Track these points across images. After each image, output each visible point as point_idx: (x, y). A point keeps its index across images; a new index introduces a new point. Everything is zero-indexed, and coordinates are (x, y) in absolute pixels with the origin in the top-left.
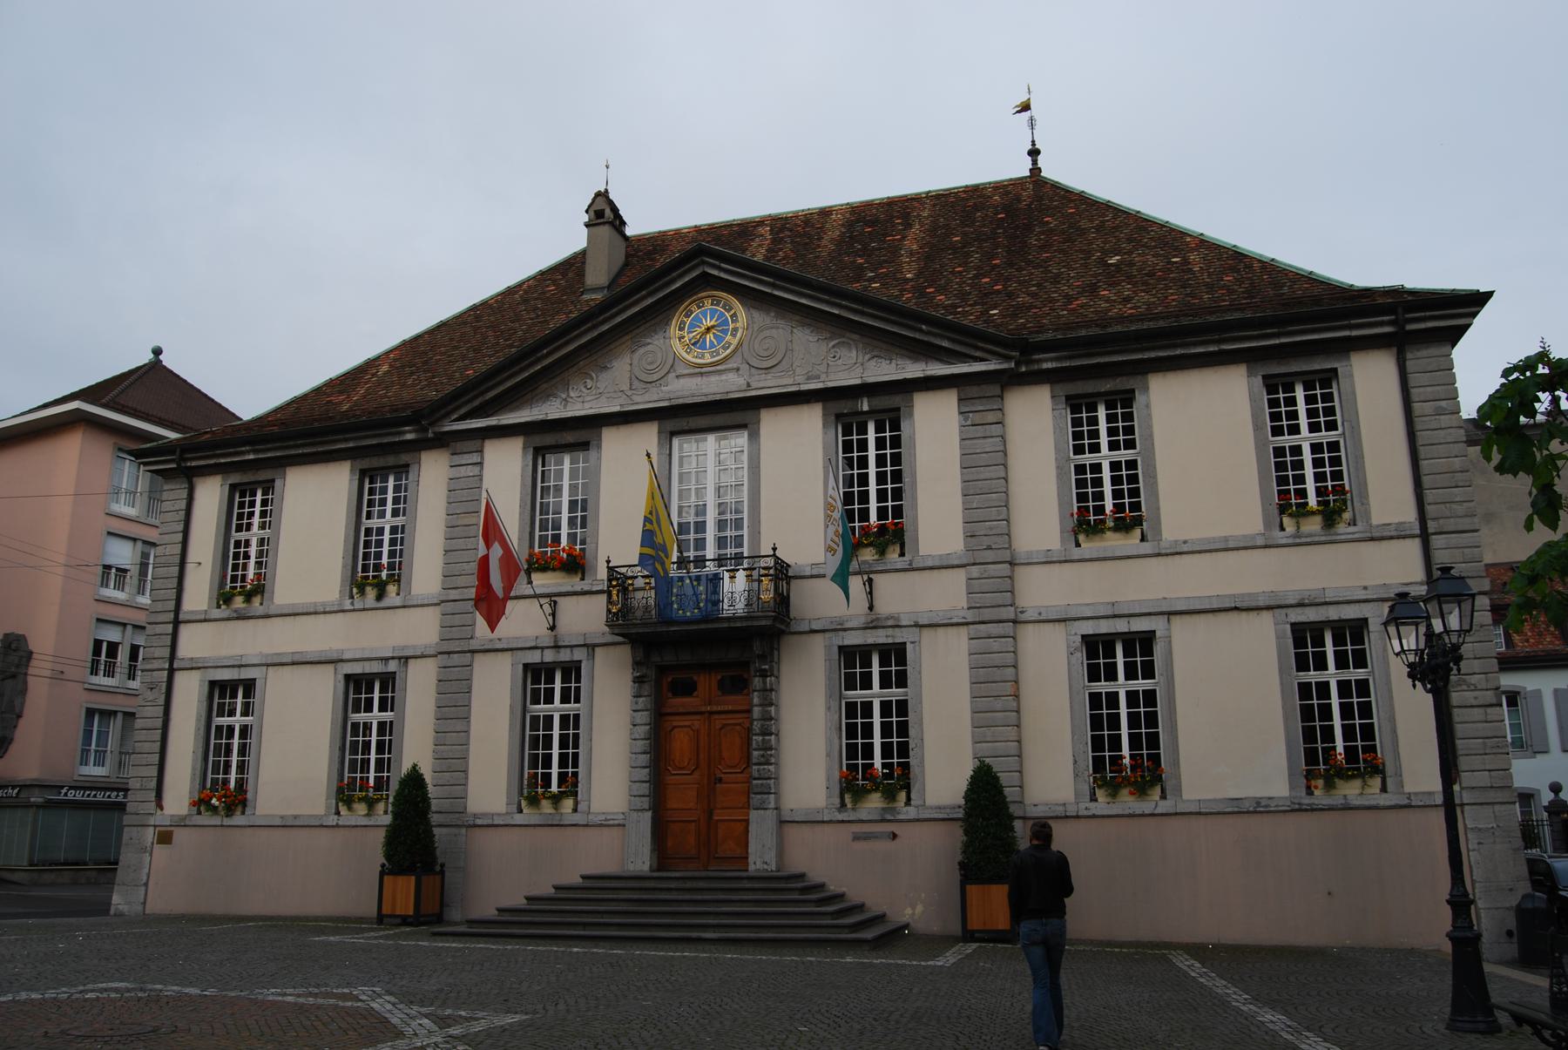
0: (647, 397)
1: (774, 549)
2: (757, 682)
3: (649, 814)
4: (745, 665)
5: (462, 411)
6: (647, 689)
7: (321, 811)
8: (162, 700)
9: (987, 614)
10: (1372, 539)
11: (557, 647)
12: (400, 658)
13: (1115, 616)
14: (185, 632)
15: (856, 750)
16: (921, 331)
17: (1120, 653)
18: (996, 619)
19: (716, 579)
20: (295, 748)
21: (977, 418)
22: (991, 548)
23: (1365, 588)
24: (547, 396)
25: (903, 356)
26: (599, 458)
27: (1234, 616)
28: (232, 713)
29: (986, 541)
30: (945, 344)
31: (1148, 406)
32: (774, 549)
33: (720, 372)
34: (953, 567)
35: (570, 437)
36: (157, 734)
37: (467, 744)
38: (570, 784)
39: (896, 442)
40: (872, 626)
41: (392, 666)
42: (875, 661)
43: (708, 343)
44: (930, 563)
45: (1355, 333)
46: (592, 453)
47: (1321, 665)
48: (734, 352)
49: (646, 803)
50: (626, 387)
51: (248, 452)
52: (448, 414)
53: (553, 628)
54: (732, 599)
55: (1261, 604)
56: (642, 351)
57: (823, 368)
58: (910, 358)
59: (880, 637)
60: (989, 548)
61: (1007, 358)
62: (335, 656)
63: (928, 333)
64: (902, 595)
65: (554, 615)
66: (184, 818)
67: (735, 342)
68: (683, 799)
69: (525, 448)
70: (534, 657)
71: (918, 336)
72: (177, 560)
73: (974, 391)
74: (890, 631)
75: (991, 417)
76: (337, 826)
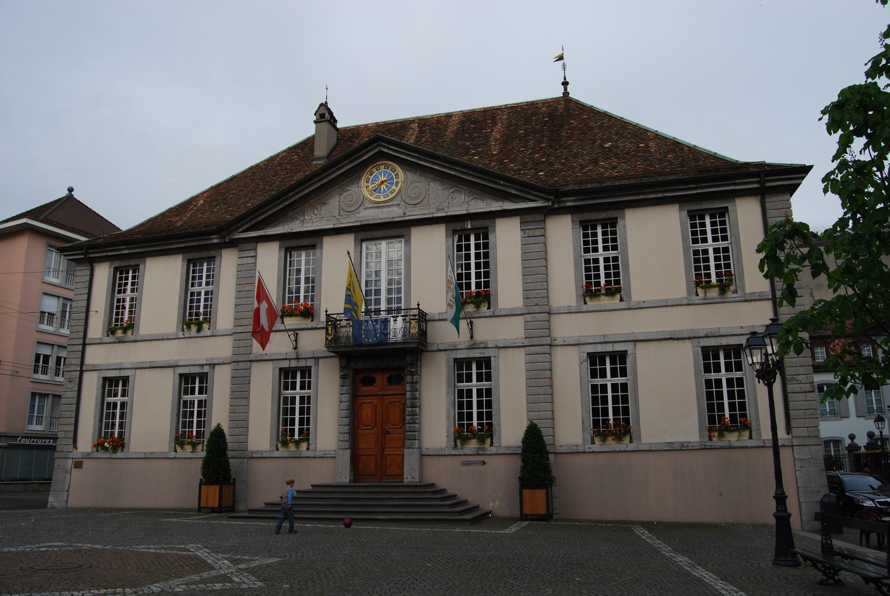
0: (348, 220)
1: (418, 305)
2: (409, 378)
3: (349, 451)
4: (402, 369)
5: (245, 227)
6: (348, 381)
7: (89, 450)
8: (76, 388)
9: (536, 341)
10: (746, 301)
11: (298, 359)
12: (210, 365)
13: (605, 342)
14: (89, 350)
15: (463, 415)
16: (500, 184)
17: (608, 363)
18: (540, 344)
19: (386, 322)
20: (151, 415)
21: (531, 233)
22: (538, 305)
23: (742, 328)
24: (293, 219)
25: (490, 198)
26: (322, 254)
27: (670, 342)
28: (116, 395)
29: (535, 301)
30: (513, 192)
31: (624, 227)
32: (418, 305)
33: (389, 206)
34: (517, 315)
35: (305, 242)
36: (74, 407)
37: (248, 412)
38: (305, 434)
39: (486, 246)
40: (473, 347)
41: (206, 369)
42: (475, 367)
43: (382, 190)
44: (504, 313)
45: (738, 188)
46: (318, 251)
47: (717, 369)
48: (397, 195)
49: (347, 445)
50: (336, 214)
51: (124, 249)
52: (237, 229)
53: (295, 348)
54: (395, 333)
55: (685, 336)
56: (345, 194)
57: (446, 204)
58: (494, 199)
59: (476, 354)
60: (537, 305)
61: (547, 200)
62: (173, 364)
63: (504, 186)
64: (489, 330)
65: (296, 341)
66: (89, 454)
67: (397, 189)
68: (368, 443)
69: (280, 248)
70: (285, 364)
71: (498, 187)
72: (84, 309)
73: (529, 218)
74: (482, 350)
75: (538, 232)
76: (175, 458)
